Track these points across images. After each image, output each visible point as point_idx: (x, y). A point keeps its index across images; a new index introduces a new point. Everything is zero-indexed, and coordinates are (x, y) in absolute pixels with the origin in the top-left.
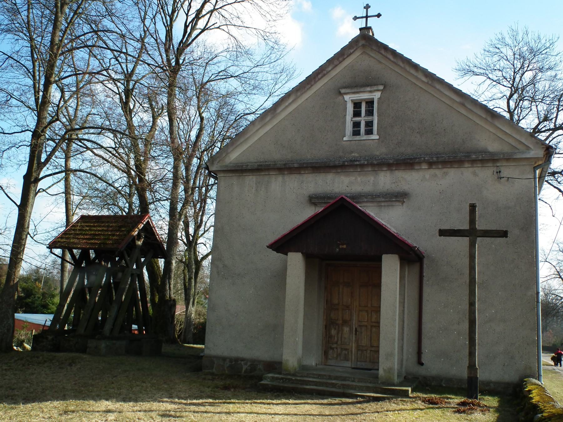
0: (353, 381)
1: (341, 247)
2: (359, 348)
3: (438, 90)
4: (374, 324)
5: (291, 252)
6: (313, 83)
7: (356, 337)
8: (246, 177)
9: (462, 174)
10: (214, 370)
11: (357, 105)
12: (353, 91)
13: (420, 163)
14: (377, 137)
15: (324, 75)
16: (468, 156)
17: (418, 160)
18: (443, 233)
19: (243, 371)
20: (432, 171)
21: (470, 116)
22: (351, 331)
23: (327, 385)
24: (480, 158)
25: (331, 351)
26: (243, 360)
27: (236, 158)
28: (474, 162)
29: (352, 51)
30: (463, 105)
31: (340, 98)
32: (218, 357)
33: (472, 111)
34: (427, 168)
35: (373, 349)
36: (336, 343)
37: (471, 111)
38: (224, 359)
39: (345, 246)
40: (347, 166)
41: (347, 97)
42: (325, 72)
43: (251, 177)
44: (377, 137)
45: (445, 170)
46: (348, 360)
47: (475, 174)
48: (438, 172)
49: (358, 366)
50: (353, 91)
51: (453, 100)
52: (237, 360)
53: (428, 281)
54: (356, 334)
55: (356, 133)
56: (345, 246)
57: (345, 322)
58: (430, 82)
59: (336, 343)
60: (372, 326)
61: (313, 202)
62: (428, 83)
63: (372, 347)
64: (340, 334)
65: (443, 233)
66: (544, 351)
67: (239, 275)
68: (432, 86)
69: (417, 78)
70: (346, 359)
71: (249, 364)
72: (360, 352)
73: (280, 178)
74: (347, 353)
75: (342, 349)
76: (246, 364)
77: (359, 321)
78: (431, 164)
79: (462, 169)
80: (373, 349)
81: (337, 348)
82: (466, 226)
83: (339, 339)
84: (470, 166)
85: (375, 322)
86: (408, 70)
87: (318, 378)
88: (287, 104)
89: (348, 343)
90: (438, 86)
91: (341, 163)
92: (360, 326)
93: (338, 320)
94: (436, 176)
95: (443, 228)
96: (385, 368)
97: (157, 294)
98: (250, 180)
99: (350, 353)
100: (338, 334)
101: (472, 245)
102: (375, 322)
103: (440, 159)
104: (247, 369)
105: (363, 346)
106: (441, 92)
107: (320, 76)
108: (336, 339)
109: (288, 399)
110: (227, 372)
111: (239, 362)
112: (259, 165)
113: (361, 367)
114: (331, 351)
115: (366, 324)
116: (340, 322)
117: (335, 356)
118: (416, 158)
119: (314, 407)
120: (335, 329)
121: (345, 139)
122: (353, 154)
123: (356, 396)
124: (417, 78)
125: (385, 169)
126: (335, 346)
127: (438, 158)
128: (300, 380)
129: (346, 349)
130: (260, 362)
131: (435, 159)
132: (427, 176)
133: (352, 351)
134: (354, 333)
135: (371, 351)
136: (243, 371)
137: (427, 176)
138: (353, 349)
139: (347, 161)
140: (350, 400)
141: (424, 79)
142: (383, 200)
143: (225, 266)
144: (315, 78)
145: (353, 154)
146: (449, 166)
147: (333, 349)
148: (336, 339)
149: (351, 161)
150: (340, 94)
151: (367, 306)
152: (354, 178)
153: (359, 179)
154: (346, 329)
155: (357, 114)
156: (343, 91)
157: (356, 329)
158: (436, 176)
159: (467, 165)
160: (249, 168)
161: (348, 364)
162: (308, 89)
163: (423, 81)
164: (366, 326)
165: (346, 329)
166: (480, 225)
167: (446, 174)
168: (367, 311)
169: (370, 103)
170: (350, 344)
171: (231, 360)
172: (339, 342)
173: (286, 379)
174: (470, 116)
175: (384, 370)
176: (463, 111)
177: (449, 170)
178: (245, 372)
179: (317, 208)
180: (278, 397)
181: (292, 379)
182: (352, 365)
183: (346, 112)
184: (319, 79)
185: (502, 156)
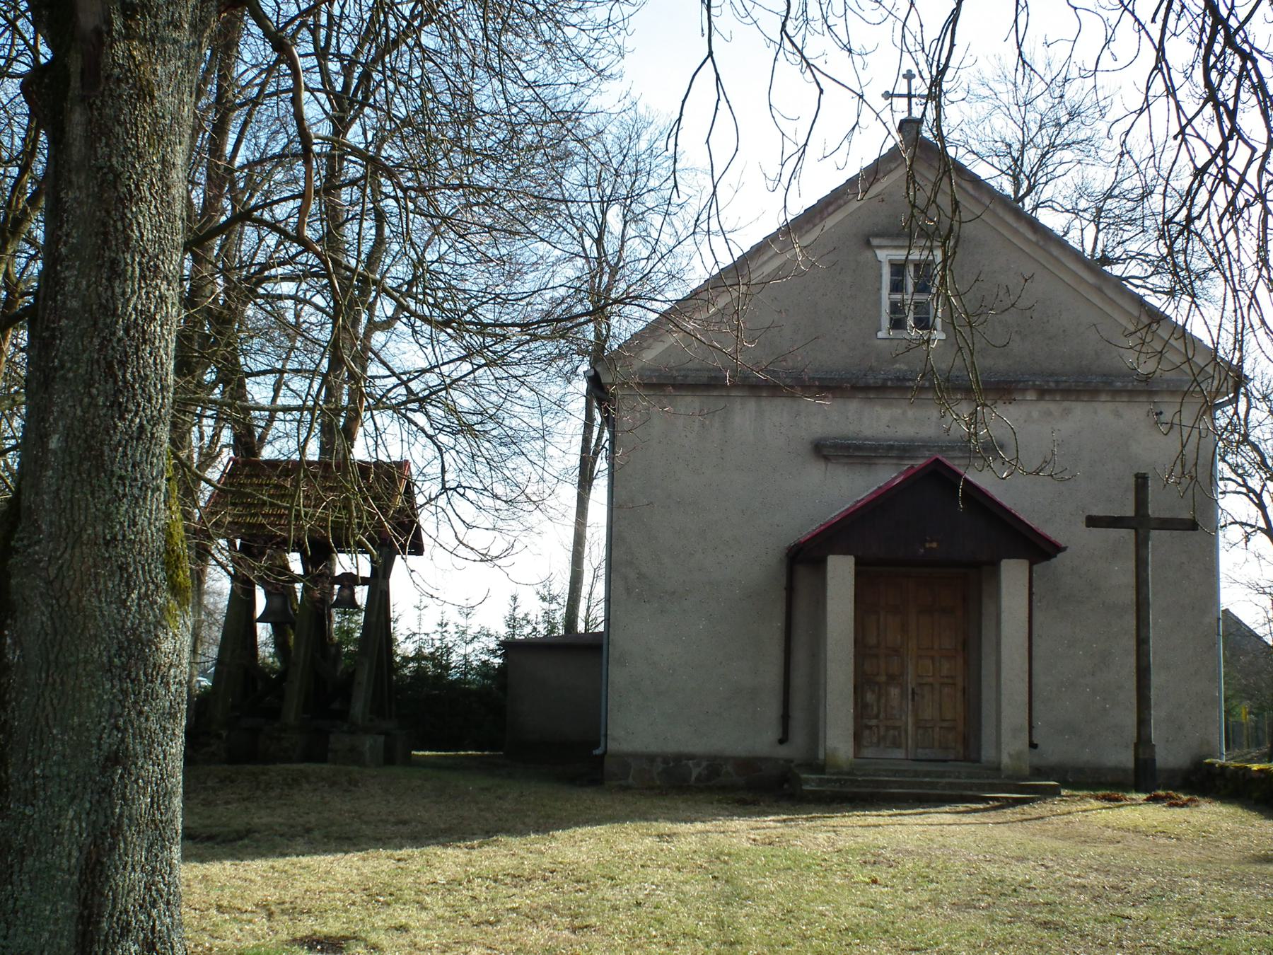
0: (958, 777)
1: (927, 545)
2: (919, 724)
3: (1056, 259)
4: (946, 680)
5: (834, 553)
6: (817, 221)
7: (913, 705)
8: (679, 398)
9: (1096, 412)
10: (630, 780)
11: (898, 269)
12: (895, 243)
13: (1024, 390)
14: (943, 336)
15: (840, 207)
16: (1111, 384)
17: (1022, 384)
18: (1092, 522)
19: (693, 778)
20: (1043, 406)
21: (1108, 309)
22: (903, 694)
23: (920, 785)
24: (1130, 387)
25: (867, 733)
26: (691, 757)
27: (655, 359)
28: (1115, 393)
29: (893, 166)
30: (1099, 290)
31: (869, 254)
32: (636, 756)
33: (1115, 302)
34: (1034, 398)
35: (945, 724)
36: (877, 717)
37: (1112, 301)
38: (651, 758)
39: (934, 545)
40: (891, 388)
41: (883, 255)
42: (841, 202)
43: (689, 399)
44: (943, 336)
45: (1066, 404)
46: (899, 747)
47: (1118, 415)
48: (1052, 407)
49: (920, 756)
50: (895, 243)
51: (1081, 277)
52: (679, 758)
53: (1040, 601)
54: (913, 699)
55: (897, 324)
56: (934, 545)
57: (892, 679)
58: (1041, 243)
59: (877, 717)
60: (942, 684)
61: (825, 453)
62: (1037, 244)
63: (943, 720)
64: (883, 701)
65: (1092, 522)
66: (231, 814)
67: (674, 593)
68: (1045, 250)
69: (1016, 231)
70: (896, 744)
71: (704, 764)
72: (920, 731)
73: (752, 404)
74: (896, 733)
75: (888, 728)
76: (698, 765)
77: (919, 676)
78: (1043, 393)
79: (1095, 404)
80: (945, 724)
81: (877, 726)
82: (1130, 512)
83: (882, 710)
84: (1109, 399)
85: (947, 677)
86: (1001, 215)
87: (895, 776)
88: (765, 258)
89: (898, 717)
90: (1056, 251)
91: (880, 382)
92: (920, 685)
93: (878, 674)
94: (1050, 414)
95: (1097, 511)
96: (1012, 752)
97: (291, 632)
98: (690, 403)
99: (903, 734)
100: (878, 700)
101: (1141, 545)
102: (947, 677)
103: (1062, 386)
104: (700, 774)
105: (926, 720)
106: (1063, 264)
107: (831, 209)
108: (875, 709)
109: (880, 810)
110: (658, 782)
111: (684, 762)
112: (711, 378)
113: (924, 758)
114: (867, 733)
115: (931, 680)
116: (883, 678)
117: (875, 740)
118: (1019, 381)
119: (945, 816)
120: (873, 692)
121: (880, 335)
122: (897, 366)
123: (985, 800)
124: (1016, 231)
125: (959, 396)
126: (874, 722)
127: (1057, 382)
128: (872, 781)
129: (895, 728)
130: (727, 759)
131: (1052, 385)
132: (1035, 414)
133: (906, 731)
134: (910, 697)
135: (941, 728)
136: (693, 778)
137: (1035, 414)
138: (909, 728)
139: (891, 379)
140: (981, 806)
141: (1030, 235)
142: (961, 455)
143: (641, 576)
144: (821, 211)
145: (897, 366)
146: (1073, 398)
147: (870, 728)
148: (875, 709)
149: (898, 379)
150: (868, 244)
151: (932, 648)
152: (899, 411)
153: (910, 413)
154: (894, 692)
155: (897, 287)
156: (875, 242)
157: (913, 689)
158: (1050, 414)
159: (1103, 397)
160: (689, 381)
161: (899, 754)
162: (807, 232)
163: (1028, 240)
164: (932, 685)
165: (894, 692)
166: (1155, 509)
167: (1067, 411)
168: (932, 658)
169: (923, 269)
170: (903, 718)
171: (666, 759)
172: (882, 715)
173: (846, 781)
174: (1108, 309)
175: (1010, 756)
176: (1096, 300)
177: (1074, 404)
178: (698, 779)
179: (830, 464)
180: (855, 808)
181: (857, 781)
182: (907, 754)
183: (881, 283)
184: (830, 215)
185: (1165, 386)
